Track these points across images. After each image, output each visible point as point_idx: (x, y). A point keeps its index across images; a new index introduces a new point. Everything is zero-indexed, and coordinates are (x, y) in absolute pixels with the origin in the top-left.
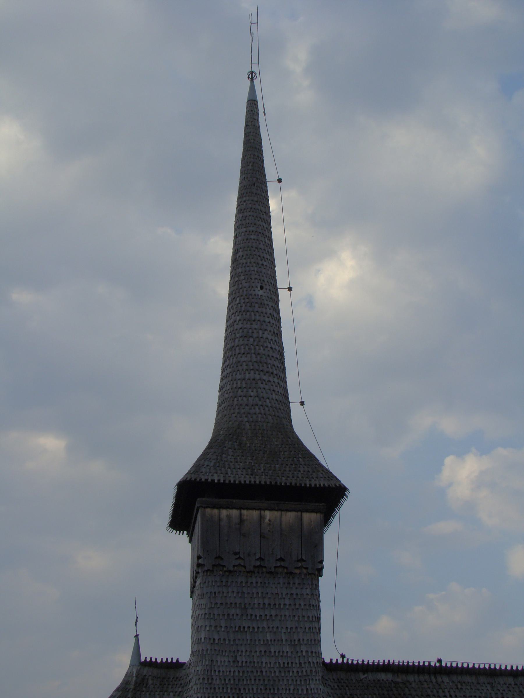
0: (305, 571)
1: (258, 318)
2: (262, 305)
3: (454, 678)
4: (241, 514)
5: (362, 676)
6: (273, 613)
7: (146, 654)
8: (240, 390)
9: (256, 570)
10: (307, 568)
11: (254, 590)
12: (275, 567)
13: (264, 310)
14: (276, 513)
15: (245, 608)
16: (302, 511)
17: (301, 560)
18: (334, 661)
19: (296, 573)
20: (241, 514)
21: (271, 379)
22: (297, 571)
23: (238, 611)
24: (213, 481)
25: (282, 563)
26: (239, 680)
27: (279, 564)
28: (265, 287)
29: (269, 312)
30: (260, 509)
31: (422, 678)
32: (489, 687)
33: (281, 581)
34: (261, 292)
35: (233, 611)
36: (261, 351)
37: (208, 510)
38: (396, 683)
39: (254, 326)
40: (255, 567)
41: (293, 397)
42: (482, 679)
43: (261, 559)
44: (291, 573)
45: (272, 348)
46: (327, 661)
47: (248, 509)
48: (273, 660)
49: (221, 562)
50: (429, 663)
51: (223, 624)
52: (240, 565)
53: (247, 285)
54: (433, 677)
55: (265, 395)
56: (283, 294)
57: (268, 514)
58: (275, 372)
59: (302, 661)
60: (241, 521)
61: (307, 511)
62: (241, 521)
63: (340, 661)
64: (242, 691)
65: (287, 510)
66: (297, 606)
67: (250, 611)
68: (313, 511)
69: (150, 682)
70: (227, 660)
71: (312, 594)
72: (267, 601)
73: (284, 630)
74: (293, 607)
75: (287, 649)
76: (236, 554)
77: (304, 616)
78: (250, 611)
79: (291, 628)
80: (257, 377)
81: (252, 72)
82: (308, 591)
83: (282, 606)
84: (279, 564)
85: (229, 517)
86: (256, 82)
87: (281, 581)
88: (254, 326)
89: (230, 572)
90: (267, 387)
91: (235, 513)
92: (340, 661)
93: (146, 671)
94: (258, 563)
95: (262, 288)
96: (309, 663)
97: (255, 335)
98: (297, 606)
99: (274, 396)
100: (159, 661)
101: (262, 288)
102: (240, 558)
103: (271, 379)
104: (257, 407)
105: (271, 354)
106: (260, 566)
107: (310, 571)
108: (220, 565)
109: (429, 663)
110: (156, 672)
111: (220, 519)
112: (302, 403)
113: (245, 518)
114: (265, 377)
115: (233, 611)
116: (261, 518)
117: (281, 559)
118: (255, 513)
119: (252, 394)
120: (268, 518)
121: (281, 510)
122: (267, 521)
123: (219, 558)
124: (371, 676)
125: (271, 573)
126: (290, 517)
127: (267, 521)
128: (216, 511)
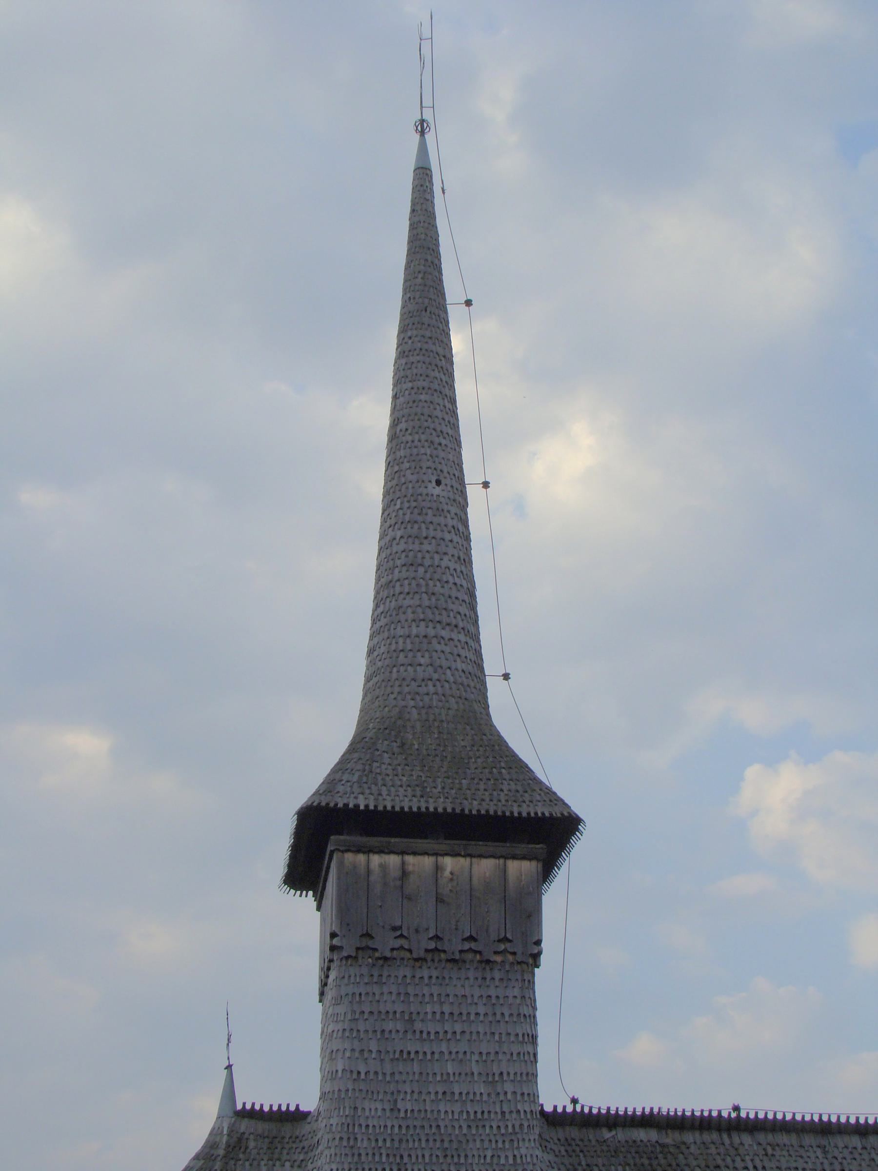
0: (510, 958)
1: (432, 533)
2: (439, 512)
3: (761, 1137)
4: (403, 863)
5: (607, 1134)
6: (458, 1028)
7: (245, 1098)
8: (402, 655)
9: (429, 957)
10: (514, 954)
11: (426, 991)
12: (461, 952)
13: (442, 520)
14: (462, 860)
15: (411, 1021)
16: (506, 858)
17: (505, 940)
18: (560, 1110)
19: (495, 962)
20: (403, 863)
21: (454, 636)
22: (498, 958)
23: (399, 1026)
24: (357, 806)
25: (473, 945)
26: (401, 1141)
27: (467, 946)
28: (443, 482)
29: (450, 523)
30: (436, 854)
31: (707, 1137)
32: (819, 1153)
33: (471, 974)
34: (437, 491)
35: (390, 1025)
36: (438, 589)
37: (349, 856)
38: (663, 1146)
39: (426, 547)
40: (427, 951)
41: (492, 666)
42: (809, 1140)
43: (437, 937)
44: (488, 962)
45: (455, 584)
46: (548, 1108)
47: (415, 853)
48: (457, 1108)
49: (371, 944)
50: (720, 1112)
51: (373, 1046)
52: (402, 948)
53: (414, 478)
54: (725, 1136)
55: (445, 664)
56: (473, 493)
57: (449, 863)
58: (461, 625)
59: (506, 1108)
60: (405, 874)
61: (514, 857)
62: (405, 874)
63: (570, 1109)
64: (406, 1159)
65: (481, 856)
66: (498, 1017)
67: (418, 1026)
68: (524, 858)
69: (252, 1144)
70: (380, 1107)
71: (523, 997)
72: (447, 1009)
73: (476, 1057)
74: (490, 1018)
75: (481, 1088)
76: (395, 929)
77: (509, 1034)
78: (418, 1026)
79: (488, 1054)
80: (431, 632)
81: (422, 121)
82: (517, 992)
83: (472, 1017)
84: (467, 946)
85: (383, 867)
86: (429, 137)
87: (471, 974)
88: (426, 547)
89: (386, 959)
90: (447, 649)
91: (393, 860)
92: (570, 1109)
93: (244, 1125)
94: (432, 945)
95: (438, 483)
96: (518, 1112)
97: (427, 562)
98: (498, 1017)
99: (460, 665)
100: (266, 1109)
101: (438, 483)
102: (402, 936)
103: (454, 636)
104: (430, 683)
105: (454, 593)
106: (436, 950)
107: (519, 958)
108: (368, 948)
109: (720, 1112)
110: (261, 1127)
111: (369, 872)
112: (506, 677)
113: (410, 868)
114: (445, 633)
115: (390, 1025)
116: (438, 868)
117: (471, 938)
118: (427, 861)
119: (422, 661)
120: (448, 870)
121: (471, 856)
122: (447, 873)
123: (368, 935)
124: (621, 1135)
125: (454, 961)
126: (485, 867)
127: (447, 873)
128: (361, 858)
